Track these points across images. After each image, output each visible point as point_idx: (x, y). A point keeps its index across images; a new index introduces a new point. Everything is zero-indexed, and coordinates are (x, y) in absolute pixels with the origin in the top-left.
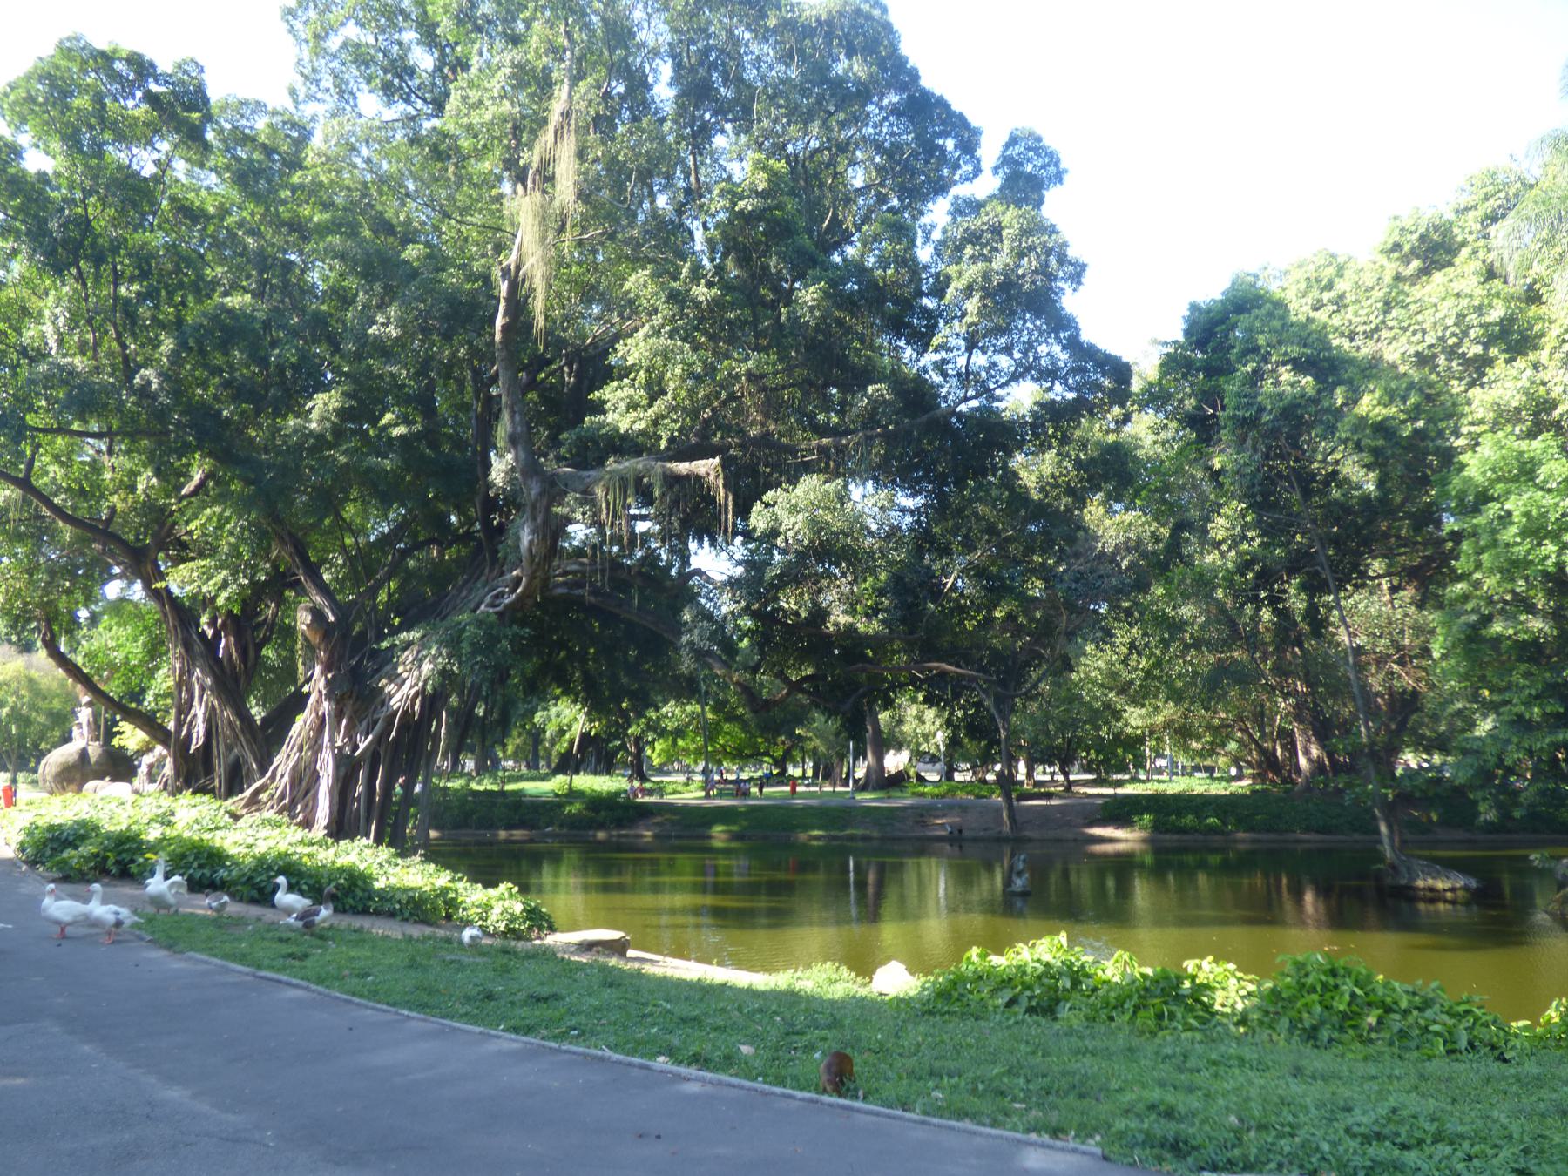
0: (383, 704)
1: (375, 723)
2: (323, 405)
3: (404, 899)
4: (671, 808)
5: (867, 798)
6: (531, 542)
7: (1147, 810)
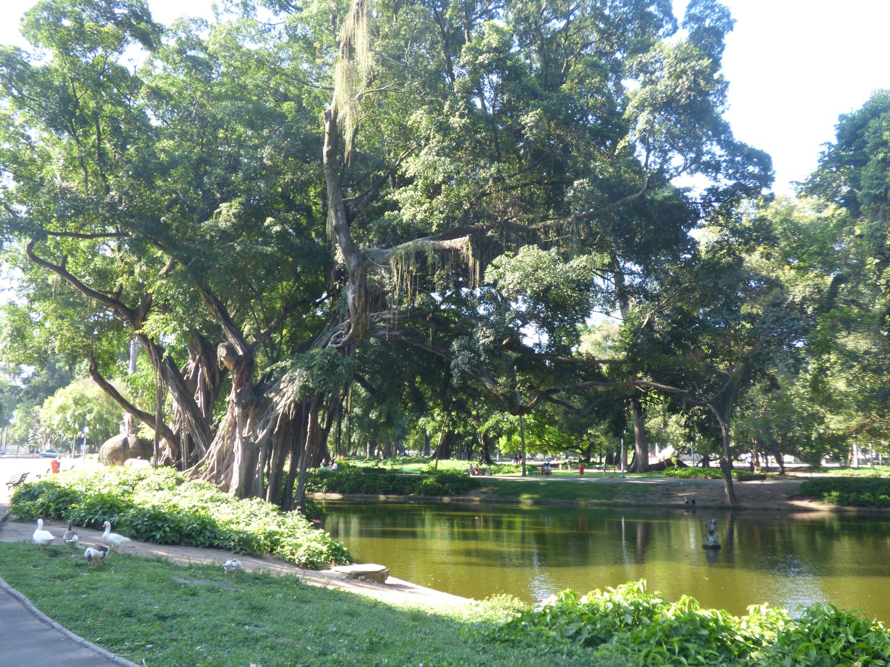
0: (273, 409)
1: (268, 421)
2: (227, 213)
3: (236, 538)
4: (495, 482)
5: (634, 478)
6: (354, 299)
7: (835, 488)
